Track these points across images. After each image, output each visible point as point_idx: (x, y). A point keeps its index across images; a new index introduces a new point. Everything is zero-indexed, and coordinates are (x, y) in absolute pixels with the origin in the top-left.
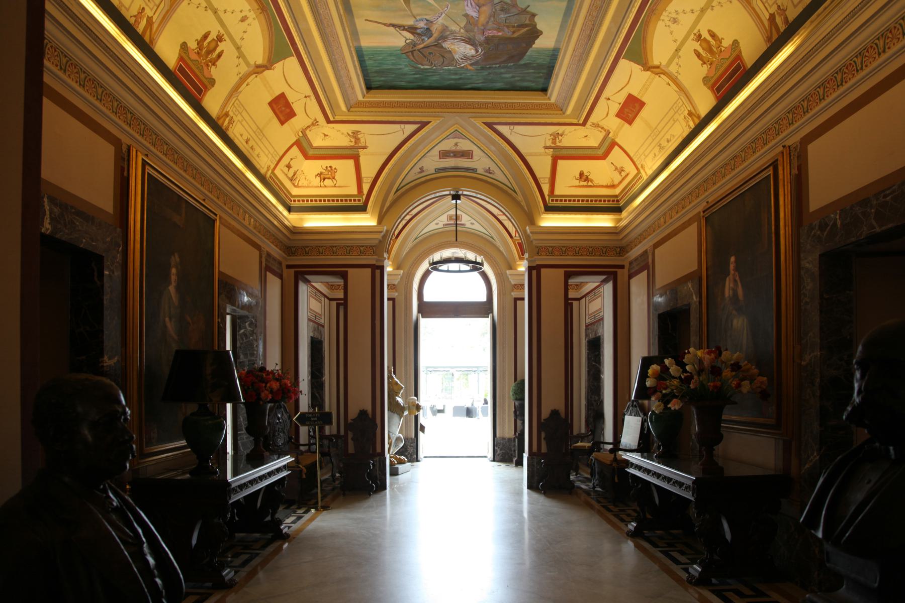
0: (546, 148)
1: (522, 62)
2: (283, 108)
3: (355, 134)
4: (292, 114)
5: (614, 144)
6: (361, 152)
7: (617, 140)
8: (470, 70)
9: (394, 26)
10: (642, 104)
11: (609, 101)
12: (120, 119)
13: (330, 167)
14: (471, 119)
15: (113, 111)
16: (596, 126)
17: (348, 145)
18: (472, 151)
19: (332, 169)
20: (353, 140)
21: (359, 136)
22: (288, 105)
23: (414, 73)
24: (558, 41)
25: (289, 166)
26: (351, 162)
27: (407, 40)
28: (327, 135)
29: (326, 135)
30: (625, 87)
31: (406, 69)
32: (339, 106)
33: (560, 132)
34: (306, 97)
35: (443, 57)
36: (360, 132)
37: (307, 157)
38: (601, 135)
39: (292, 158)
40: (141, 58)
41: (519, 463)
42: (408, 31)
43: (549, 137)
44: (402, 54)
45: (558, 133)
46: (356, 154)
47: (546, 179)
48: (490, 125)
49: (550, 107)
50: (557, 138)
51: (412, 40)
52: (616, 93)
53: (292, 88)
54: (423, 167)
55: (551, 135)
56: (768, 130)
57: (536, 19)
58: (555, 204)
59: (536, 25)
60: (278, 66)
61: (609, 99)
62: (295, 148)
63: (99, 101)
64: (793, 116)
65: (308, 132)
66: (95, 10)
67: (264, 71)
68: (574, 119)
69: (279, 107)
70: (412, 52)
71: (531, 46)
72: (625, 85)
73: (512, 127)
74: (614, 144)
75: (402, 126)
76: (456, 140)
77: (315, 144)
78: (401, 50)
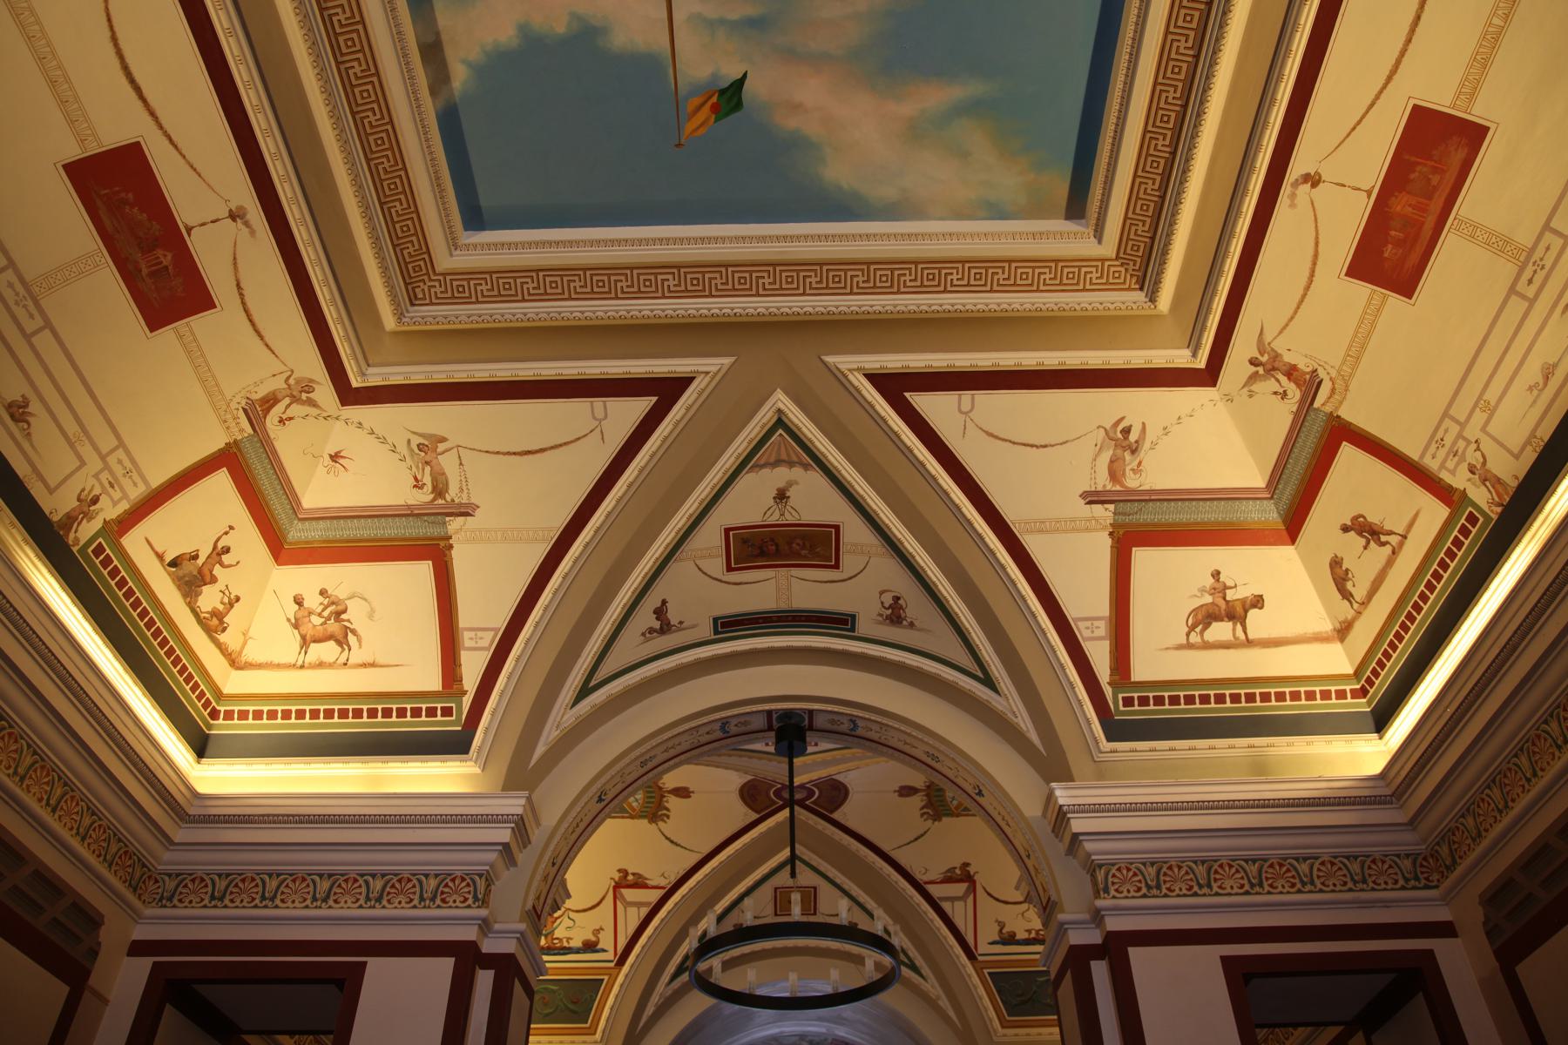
0: (1093, 498)
3: (429, 447)
7: (1346, 413)
10: (1474, 135)
12: (29, 792)
15: (105, 859)
18: (837, 528)
36: (443, 440)
40: (120, 674)
41: (365, 963)
47: (1096, 623)
48: (668, 390)
56: (1450, 834)
58: (1137, 712)
63: (79, 838)
64: (1451, 850)
66: (130, 687)
76: (781, 475)
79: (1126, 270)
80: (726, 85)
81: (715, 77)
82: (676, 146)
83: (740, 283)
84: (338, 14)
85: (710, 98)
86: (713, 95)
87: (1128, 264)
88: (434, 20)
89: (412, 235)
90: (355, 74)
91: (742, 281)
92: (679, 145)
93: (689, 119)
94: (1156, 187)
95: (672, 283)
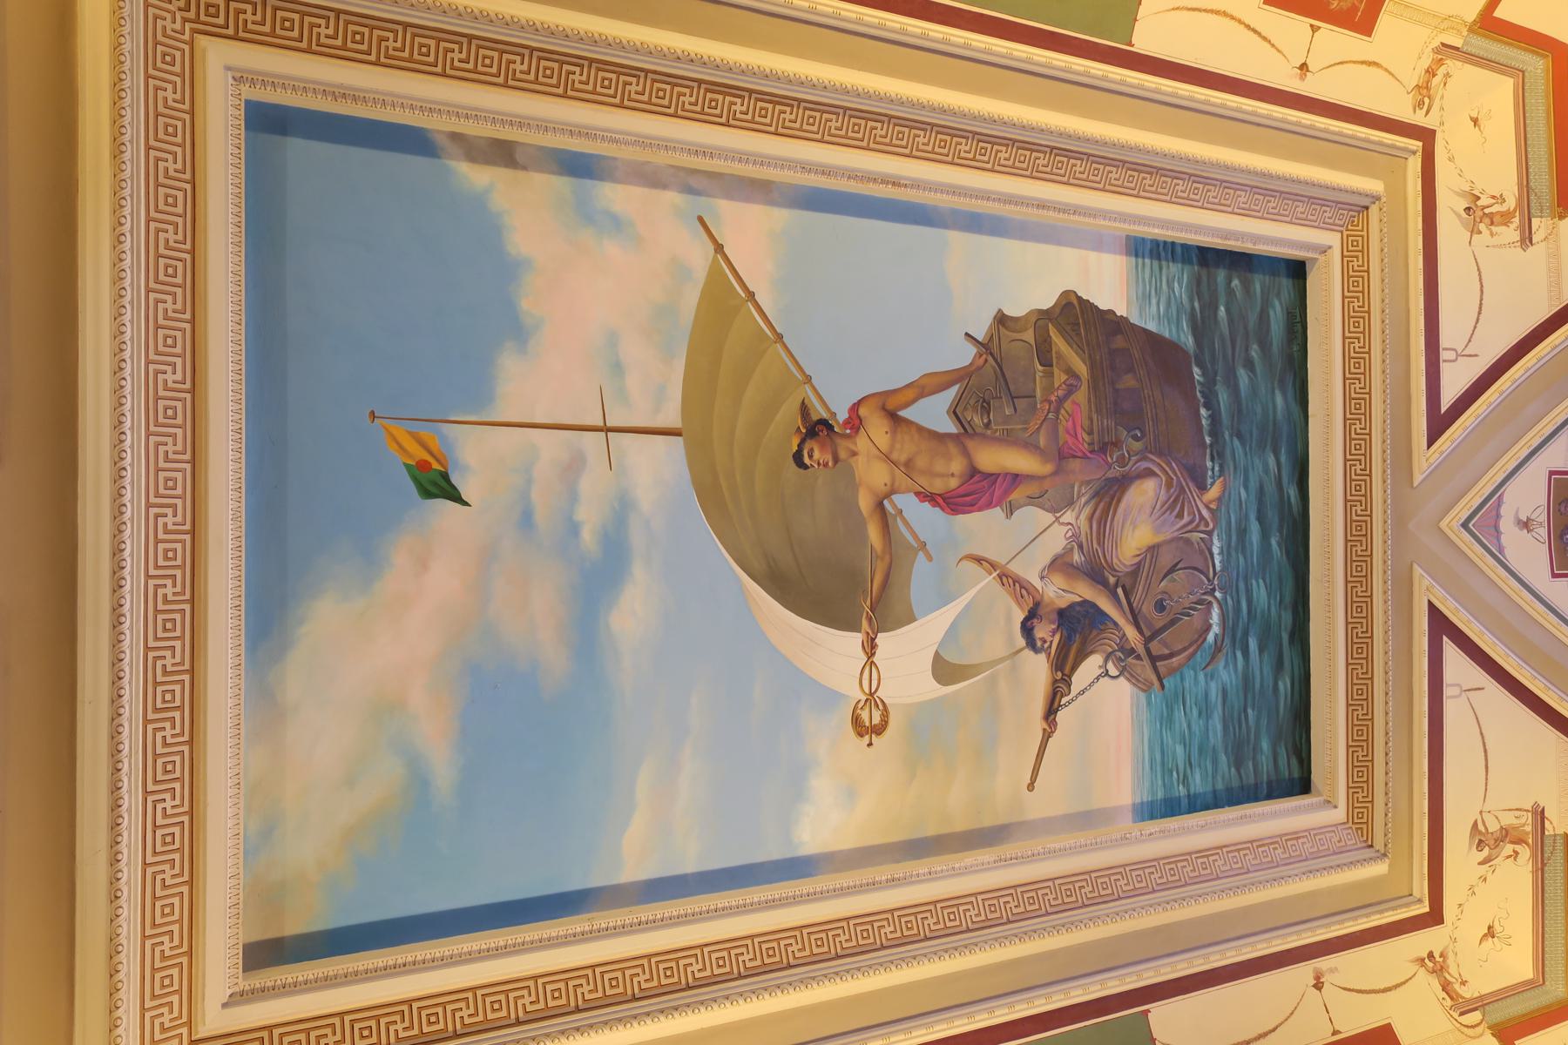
0: (1527, 239)
1: (1188, 341)
3: (1480, 838)
5: (1489, 24)
9: (1051, 712)
16: (1423, 93)
18: (1551, 473)
20: (1508, 849)
21: (1493, 827)
23: (1239, 654)
24: (1098, 243)
28: (1489, 928)
29: (1491, 933)
31: (1226, 674)
34: (1318, 986)
35: (1172, 570)
36: (1475, 824)
38: (1462, 74)
42: (1074, 668)
44: (1163, 686)
45: (1468, 209)
48: (1439, 423)
50: (1487, 211)
51: (1106, 661)
55: (1474, 231)
57: (1015, 310)
59: (1040, 312)
61: (1304, 67)
65: (1467, 993)
70: (1154, 659)
71: (1124, 319)
73: (1444, 355)
74: (1489, 24)
76: (1507, 525)
77: (1526, 972)
78: (1146, 688)
80: (455, 480)
83: (167, 480)
84: (581, 75)
85: (438, 461)
86: (444, 468)
88: (541, 170)
89: (754, 116)
90: (919, 136)
91: (170, 484)
94: (698, 975)
95: (170, 377)
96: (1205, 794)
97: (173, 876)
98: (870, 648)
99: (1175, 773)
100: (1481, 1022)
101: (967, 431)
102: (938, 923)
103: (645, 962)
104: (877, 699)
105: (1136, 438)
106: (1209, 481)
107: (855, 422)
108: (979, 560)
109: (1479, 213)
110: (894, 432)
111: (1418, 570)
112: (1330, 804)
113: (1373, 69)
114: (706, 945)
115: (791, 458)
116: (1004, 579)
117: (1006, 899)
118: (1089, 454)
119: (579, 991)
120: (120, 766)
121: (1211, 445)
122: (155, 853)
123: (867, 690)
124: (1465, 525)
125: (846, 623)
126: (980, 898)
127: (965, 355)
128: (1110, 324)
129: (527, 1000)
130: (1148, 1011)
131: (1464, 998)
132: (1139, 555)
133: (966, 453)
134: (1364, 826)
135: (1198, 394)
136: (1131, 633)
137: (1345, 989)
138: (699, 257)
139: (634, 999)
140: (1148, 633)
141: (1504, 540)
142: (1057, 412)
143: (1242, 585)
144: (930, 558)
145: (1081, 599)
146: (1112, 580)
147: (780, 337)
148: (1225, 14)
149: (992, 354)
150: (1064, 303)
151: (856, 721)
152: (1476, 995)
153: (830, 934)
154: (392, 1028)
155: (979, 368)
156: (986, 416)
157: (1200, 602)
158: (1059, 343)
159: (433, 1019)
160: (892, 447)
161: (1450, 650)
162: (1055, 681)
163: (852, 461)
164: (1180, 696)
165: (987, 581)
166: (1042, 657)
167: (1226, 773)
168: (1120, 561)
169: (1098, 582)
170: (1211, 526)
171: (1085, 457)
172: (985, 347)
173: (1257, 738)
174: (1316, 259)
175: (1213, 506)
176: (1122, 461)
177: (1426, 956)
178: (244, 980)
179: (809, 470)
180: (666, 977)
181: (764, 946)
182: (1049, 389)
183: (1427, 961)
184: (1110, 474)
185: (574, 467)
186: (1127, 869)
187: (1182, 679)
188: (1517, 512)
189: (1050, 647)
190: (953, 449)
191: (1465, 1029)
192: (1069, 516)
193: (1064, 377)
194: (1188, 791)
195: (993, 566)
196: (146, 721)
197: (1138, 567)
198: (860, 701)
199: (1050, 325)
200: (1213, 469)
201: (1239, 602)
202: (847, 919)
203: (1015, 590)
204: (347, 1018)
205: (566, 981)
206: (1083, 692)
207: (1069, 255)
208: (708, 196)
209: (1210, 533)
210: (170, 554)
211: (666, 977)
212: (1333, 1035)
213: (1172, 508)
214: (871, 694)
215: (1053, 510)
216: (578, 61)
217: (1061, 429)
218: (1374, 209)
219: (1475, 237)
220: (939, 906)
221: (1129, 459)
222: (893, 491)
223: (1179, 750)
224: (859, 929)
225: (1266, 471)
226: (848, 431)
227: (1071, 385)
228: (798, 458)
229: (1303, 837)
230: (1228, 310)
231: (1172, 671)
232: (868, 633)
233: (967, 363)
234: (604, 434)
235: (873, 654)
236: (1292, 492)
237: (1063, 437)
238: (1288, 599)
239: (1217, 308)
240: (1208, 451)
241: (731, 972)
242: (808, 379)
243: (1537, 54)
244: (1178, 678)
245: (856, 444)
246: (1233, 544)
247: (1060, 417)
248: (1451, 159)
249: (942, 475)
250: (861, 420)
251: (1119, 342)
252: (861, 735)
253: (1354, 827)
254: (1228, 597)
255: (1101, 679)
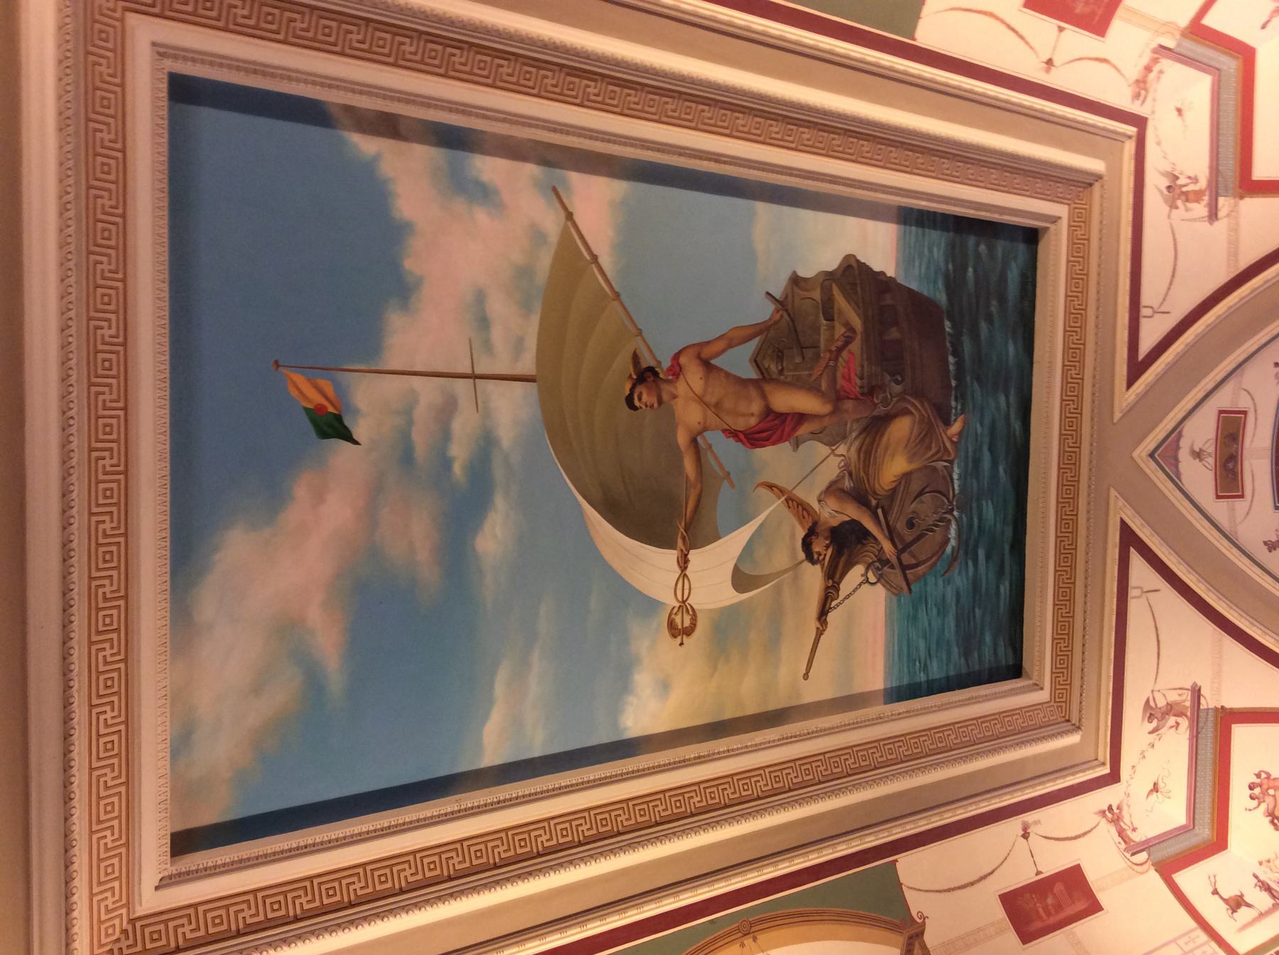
0: (1213, 215)
1: (942, 298)
2: (1050, 901)
3: (1151, 712)
4: (1074, 879)
5: (1197, 30)
6: (1209, 702)
7: (1184, 20)
8: (965, 423)
9: (823, 613)
11: (1056, 61)
13: (1251, 787)
14: (1115, 421)
16: (1141, 87)
17: (1187, 735)
18: (1221, 412)
19: (1260, 785)
20: (1172, 720)
21: (1161, 703)
22: (1042, 887)
23: (970, 563)
25: (1236, 903)
26: (1240, 732)
27: (867, 581)
28: (1155, 784)
29: (1155, 788)
30: (1002, 21)
31: (960, 580)
32: (1070, 749)
33: (1164, 183)
34: (1026, 836)
35: (921, 493)
36: (1148, 701)
37: (1219, 843)
38: (1173, 71)
39: (1211, 889)
42: (842, 577)
43: (1179, 213)
44: (910, 589)
45: (1169, 188)
46: (1216, 717)
48: (1137, 368)
49: (1080, 222)
51: (867, 570)
52: (1027, 43)
53: (992, 872)
54: (1265, 543)
55: (1173, 206)
57: (806, 272)
60: (916, 903)
61: (1049, 62)
62: (1184, 878)
65: (1137, 837)
67: (924, 947)
68: (1122, 150)
69: (1041, 910)
70: (904, 568)
72: (998, 23)
73: (1144, 312)
74: (1197, 30)
75: (1132, 593)
76: (1184, 455)
77: (1181, 819)
79: (118, 940)
80: (347, 422)
81: (356, 412)
82: (276, 362)
85: (333, 405)
86: (336, 408)
87: (127, 938)
92: (277, 363)
93: (309, 380)
96: (940, 679)
97: (113, 778)
98: (684, 562)
99: (917, 663)
100: (1146, 862)
101: (765, 378)
102: (734, 793)
103: (503, 835)
104: (689, 607)
105: (897, 382)
106: (953, 418)
107: (676, 370)
108: (771, 487)
109: (1177, 191)
110: (706, 378)
111: (1113, 493)
112: (1038, 687)
113: (1104, 65)
114: (553, 818)
115: (624, 401)
116: (790, 502)
117: (787, 771)
118: (860, 397)
119: (451, 862)
120: (71, 683)
121: (956, 386)
122: (99, 759)
123: (680, 598)
124: (1151, 455)
125: (661, 540)
126: (767, 770)
127: (763, 312)
128: (880, 283)
129: (408, 873)
130: (896, 861)
131: (1133, 841)
132: (895, 481)
133: (764, 396)
134: (1064, 704)
135: (948, 345)
136: (887, 546)
137: (1046, 837)
138: (551, 223)
139: (496, 867)
140: (900, 547)
141: (1182, 467)
142: (836, 360)
143: (974, 505)
144: (732, 485)
145: (849, 519)
146: (874, 502)
147: (617, 295)
148: (991, 15)
149: (787, 310)
150: (846, 265)
151: (671, 625)
152: (1144, 839)
153: (651, 805)
154: (297, 902)
155: (776, 323)
156: (780, 364)
157: (941, 520)
158: (841, 301)
159: (331, 892)
160: (705, 390)
161: (1136, 561)
162: (827, 588)
163: (673, 403)
164: (923, 598)
165: (776, 504)
166: (818, 567)
167: (957, 664)
168: (881, 486)
169: (863, 505)
170: (953, 456)
171: (856, 399)
172: (781, 304)
173: (982, 634)
174: (1047, 229)
175: (955, 439)
176: (885, 402)
177: (1106, 808)
178: (171, 866)
179: (639, 411)
180: (521, 847)
181: (599, 817)
182: (831, 340)
183: (1107, 813)
184: (875, 413)
185: (448, 409)
186: (881, 743)
187: (926, 584)
188: (1192, 445)
189: (824, 559)
190: (753, 392)
191: (1135, 867)
192: (842, 449)
193: (843, 330)
194: (928, 677)
195: (782, 491)
196: (91, 643)
197: (894, 491)
198: (674, 608)
199: (834, 286)
200: (956, 408)
201: (972, 519)
202: (663, 792)
203: (798, 511)
204: (260, 895)
205: (440, 854)
206: (849, 596)
207: (852, 223)
208: (562, 168)
209: (951, 462)
210: (108, 493)
211: (521, 847)
212: (1037, 875)
213: (922, 440)
214: (684, 602)
215: (830, 444)
216: (460, 45)
217: (839, 375)
218: (1097, 186)
219: (1174, 211)
220: (735, 778)
221: (891, 400)
222: (705, 429)
223: (922, 644)
224: (673, 800)
225: (998, 409)
226: (670, 377)
227: (848, 337)
228: (629, 401)
229: (1016, 714)
230: (975, 271)
231: (918, 579)
232: (682, 551)
233: (767, 318)
234: (472, 380)
235: (686, 568)
236: (1017, 426)
237: (840, 382)
238: (1010, 517)
239: (965, 269)
240: (953, 393)
241: (573, 841)
242: (640, 332)
243: (1231, 56)
244: (923, 583)
245: (676, 389)
246: (969, 470)
247: (839, 364)
248: (1159, 144)
249: (743, 415)
250: (681, 368)
251: (888, 299)
252: (674, 636)
253: (1055, 705)
254: (963, 516)
255: (863, 586)
